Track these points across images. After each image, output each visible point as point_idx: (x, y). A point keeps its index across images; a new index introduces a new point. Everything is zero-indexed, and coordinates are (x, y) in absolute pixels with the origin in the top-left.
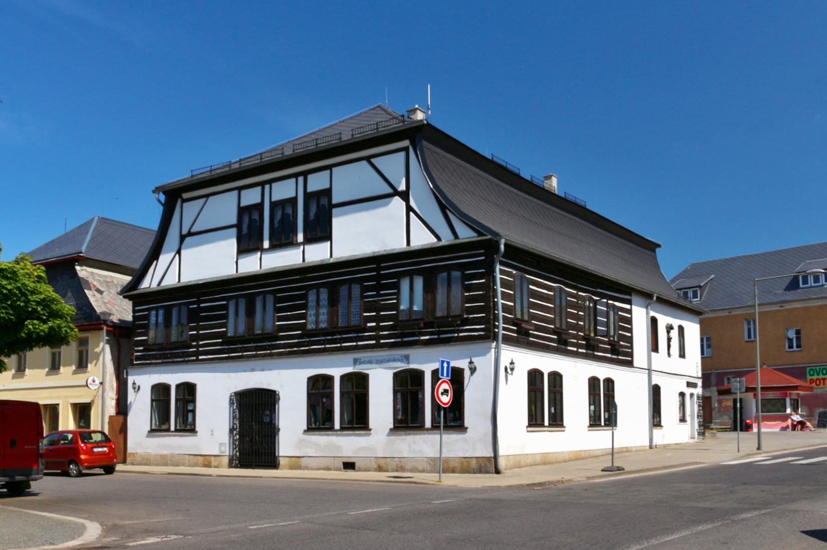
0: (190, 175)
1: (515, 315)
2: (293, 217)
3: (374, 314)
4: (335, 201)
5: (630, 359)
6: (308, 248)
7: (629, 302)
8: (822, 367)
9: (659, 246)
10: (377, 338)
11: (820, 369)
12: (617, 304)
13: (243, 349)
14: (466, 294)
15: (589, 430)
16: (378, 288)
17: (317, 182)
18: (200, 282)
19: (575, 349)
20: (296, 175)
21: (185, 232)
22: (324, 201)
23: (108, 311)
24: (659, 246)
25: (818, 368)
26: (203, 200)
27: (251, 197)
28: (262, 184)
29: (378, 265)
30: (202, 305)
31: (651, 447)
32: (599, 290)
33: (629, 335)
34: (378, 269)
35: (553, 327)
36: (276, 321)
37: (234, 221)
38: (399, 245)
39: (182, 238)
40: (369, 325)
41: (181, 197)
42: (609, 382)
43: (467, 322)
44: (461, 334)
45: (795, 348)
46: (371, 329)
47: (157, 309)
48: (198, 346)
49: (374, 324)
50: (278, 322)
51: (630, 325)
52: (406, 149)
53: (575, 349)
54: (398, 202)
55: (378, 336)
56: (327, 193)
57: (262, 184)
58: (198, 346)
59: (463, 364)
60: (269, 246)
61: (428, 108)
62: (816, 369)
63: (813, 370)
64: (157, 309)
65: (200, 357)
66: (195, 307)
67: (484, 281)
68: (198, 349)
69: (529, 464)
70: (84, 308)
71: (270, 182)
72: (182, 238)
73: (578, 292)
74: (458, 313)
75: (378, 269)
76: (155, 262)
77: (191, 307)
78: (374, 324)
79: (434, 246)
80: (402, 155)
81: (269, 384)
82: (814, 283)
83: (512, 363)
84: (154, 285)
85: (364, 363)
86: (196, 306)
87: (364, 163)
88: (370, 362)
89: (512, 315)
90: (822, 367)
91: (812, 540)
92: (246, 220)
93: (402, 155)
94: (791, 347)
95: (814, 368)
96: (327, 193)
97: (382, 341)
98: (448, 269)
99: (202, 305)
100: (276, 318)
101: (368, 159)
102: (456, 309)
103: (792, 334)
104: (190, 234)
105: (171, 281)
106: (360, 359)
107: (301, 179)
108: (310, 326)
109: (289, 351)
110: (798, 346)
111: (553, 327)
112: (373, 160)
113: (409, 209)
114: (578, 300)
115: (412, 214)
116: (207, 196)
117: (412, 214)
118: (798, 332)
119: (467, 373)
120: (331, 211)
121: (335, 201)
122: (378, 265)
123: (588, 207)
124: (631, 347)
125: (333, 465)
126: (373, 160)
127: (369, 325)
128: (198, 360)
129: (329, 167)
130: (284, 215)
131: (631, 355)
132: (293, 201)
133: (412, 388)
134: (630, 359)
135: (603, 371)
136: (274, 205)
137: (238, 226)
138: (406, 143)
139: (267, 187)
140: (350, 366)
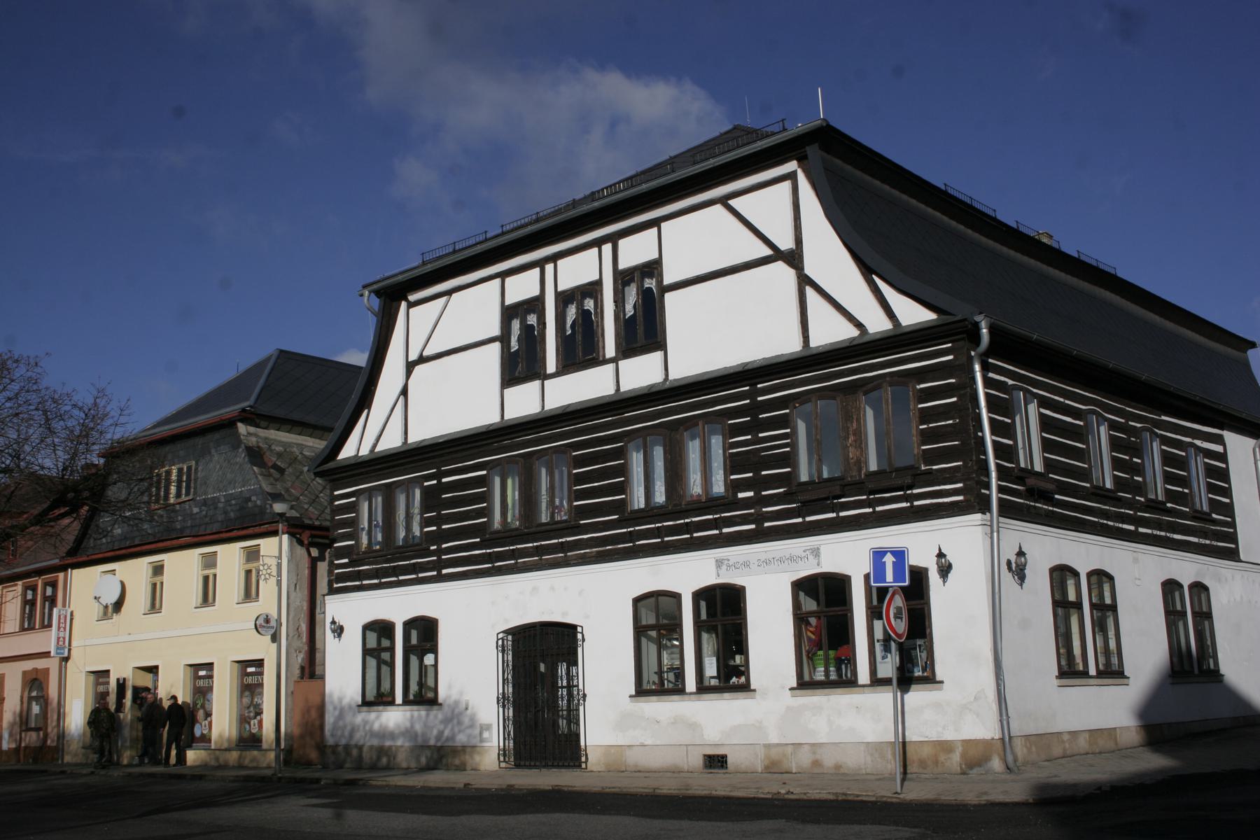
0: (421, 262)
1: (1018, 463)
2: (596, 313)
3: (751, 475)
4: (667, 280)
5: (1233, 546)
6: (624, 364)
7: (1219, 440)
9: (1253, 345)
10: (759, 519)
12: (1198, 442)
13: (571, 207)
15: (1173, 684)
17: (635, 251)
18: (441, 441)
19: (1132, 528)
20: (598, 243)
21: (413, 356)
22: (650, 283)
24: (1253, 345)
26: (444, 299)
27: (522, 287)
28: (540, 264)
30: (444, 480)
32: (1163, 418)
33: (1227, 501)
34: (752, 395)
35: (1088, 485)
36: (573, 499)
37: (496, 331)
38: (790, 345)
39: (410, 367)
40: (741, 495)
41: (407, 300)
42: (1199, 589)
46: (746, 503)
47: (370, 493)
48: (440, 552)
49: (751, 494)
50: (576, 501)
51: (1226, 483)
52: (792, 176)
53: (1132, 528)
54: (782, 273)
55: (758, 515)
56: (652, 268)
57: (540, 264)
58: (440, 552)
59: (921, 557)
60: (557, 368)
64: (370, 493)
65: (444, 571)
66: (446, 524)
67: (954, 399)
68: (439, 558)
69: (1082, 752)
70: (254, 498)
71: (554, 258)
72: (410, 367)
73: (1127, 421)
75: (752, 395)
76: (366, 411)
77: (426, 484)
78: (751, 494)
79: (855, 343)
80: (787, 185)
81: (565, 614)
83: (1021, 553)
84: (365, 451)
85: (735, 566)
86: (435, 482)
87: (718, 208)
88: (746, 564)
89: (1012, 463)
91: (143, 672)
92: (516, 325)
96: (652, 268)
97: (766, 524)
99: (444, 480)
100: (573, 495)
101: (724, 201)
104: (422, 360)
105: (392, 441)
106: (729, 560)
107: (607, 248)
108: (639, 501)
109: (598, 552)
111: (1088, 485)
112: (732, 202)
113: (804, 281)
114: (1129, 437)
115: (810, 292)
116: (449, 293)
117: (810, 292)
119: (934, 577)
120: (664, 296)
121: (667, 280)
123: (1120, 275)
124: (1233, 524)
125: (685, 759)
126: (732, 202)
127: (741, 495)
128: (440, 578)
129: (656, 223)
130: (584, 315)
131: (1233, 538)
132: (593, 289)
133: (828, 609)
134: (1233, 546)
135: (1187, 568)
136: (564, 298)
137: (504, 339)
138: (792, 166)
139: (549, 268)
140: (878, 466)
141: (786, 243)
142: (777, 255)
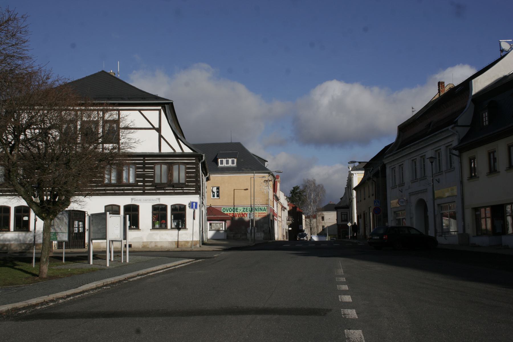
8: (229, 208)
11: (228, 209)
14: (187, 175)
16: (144, 168)
23: (426, 201)
24: (267, 161)
25: (227, 208)
29: (144, 160)
31: (391, 208)
38: (156, 151)
43: (188, 186)
44: (175, 191)
45: (216, 197)
46: (140, 186)
61: (118, 73)
62: (226, 209)
63: (224, 209)
74: (184, 182)
80: (158, 112)
82: (232, 164)
87: (138, 112)
90: (229, 208)
93: (158, 112)
94: (214, 196)
95: (225, 208)
98: (179, 164)
101: (140, 110)
102: (182, 181)
103: (215, 190)
110: (218, 196)
113: (160, 136)
115: (152, 127)
118: (218, 188)
122: (144, 160)
138: (160, 108)
141: (157, 126)
142: (154, 128)
